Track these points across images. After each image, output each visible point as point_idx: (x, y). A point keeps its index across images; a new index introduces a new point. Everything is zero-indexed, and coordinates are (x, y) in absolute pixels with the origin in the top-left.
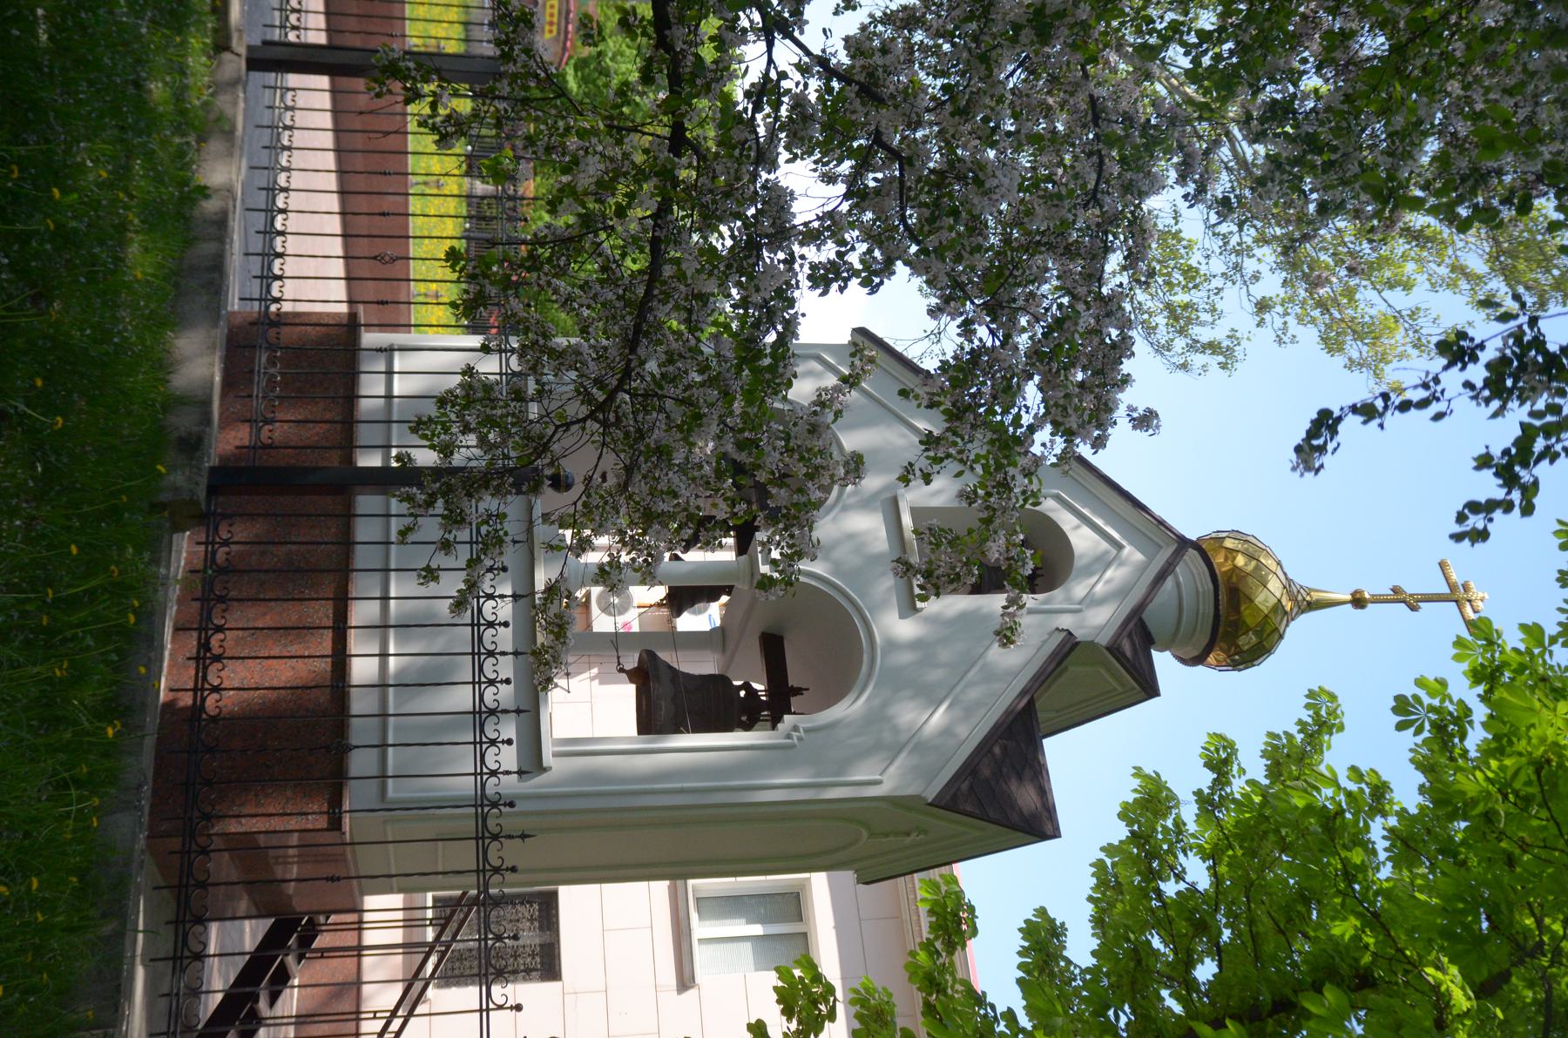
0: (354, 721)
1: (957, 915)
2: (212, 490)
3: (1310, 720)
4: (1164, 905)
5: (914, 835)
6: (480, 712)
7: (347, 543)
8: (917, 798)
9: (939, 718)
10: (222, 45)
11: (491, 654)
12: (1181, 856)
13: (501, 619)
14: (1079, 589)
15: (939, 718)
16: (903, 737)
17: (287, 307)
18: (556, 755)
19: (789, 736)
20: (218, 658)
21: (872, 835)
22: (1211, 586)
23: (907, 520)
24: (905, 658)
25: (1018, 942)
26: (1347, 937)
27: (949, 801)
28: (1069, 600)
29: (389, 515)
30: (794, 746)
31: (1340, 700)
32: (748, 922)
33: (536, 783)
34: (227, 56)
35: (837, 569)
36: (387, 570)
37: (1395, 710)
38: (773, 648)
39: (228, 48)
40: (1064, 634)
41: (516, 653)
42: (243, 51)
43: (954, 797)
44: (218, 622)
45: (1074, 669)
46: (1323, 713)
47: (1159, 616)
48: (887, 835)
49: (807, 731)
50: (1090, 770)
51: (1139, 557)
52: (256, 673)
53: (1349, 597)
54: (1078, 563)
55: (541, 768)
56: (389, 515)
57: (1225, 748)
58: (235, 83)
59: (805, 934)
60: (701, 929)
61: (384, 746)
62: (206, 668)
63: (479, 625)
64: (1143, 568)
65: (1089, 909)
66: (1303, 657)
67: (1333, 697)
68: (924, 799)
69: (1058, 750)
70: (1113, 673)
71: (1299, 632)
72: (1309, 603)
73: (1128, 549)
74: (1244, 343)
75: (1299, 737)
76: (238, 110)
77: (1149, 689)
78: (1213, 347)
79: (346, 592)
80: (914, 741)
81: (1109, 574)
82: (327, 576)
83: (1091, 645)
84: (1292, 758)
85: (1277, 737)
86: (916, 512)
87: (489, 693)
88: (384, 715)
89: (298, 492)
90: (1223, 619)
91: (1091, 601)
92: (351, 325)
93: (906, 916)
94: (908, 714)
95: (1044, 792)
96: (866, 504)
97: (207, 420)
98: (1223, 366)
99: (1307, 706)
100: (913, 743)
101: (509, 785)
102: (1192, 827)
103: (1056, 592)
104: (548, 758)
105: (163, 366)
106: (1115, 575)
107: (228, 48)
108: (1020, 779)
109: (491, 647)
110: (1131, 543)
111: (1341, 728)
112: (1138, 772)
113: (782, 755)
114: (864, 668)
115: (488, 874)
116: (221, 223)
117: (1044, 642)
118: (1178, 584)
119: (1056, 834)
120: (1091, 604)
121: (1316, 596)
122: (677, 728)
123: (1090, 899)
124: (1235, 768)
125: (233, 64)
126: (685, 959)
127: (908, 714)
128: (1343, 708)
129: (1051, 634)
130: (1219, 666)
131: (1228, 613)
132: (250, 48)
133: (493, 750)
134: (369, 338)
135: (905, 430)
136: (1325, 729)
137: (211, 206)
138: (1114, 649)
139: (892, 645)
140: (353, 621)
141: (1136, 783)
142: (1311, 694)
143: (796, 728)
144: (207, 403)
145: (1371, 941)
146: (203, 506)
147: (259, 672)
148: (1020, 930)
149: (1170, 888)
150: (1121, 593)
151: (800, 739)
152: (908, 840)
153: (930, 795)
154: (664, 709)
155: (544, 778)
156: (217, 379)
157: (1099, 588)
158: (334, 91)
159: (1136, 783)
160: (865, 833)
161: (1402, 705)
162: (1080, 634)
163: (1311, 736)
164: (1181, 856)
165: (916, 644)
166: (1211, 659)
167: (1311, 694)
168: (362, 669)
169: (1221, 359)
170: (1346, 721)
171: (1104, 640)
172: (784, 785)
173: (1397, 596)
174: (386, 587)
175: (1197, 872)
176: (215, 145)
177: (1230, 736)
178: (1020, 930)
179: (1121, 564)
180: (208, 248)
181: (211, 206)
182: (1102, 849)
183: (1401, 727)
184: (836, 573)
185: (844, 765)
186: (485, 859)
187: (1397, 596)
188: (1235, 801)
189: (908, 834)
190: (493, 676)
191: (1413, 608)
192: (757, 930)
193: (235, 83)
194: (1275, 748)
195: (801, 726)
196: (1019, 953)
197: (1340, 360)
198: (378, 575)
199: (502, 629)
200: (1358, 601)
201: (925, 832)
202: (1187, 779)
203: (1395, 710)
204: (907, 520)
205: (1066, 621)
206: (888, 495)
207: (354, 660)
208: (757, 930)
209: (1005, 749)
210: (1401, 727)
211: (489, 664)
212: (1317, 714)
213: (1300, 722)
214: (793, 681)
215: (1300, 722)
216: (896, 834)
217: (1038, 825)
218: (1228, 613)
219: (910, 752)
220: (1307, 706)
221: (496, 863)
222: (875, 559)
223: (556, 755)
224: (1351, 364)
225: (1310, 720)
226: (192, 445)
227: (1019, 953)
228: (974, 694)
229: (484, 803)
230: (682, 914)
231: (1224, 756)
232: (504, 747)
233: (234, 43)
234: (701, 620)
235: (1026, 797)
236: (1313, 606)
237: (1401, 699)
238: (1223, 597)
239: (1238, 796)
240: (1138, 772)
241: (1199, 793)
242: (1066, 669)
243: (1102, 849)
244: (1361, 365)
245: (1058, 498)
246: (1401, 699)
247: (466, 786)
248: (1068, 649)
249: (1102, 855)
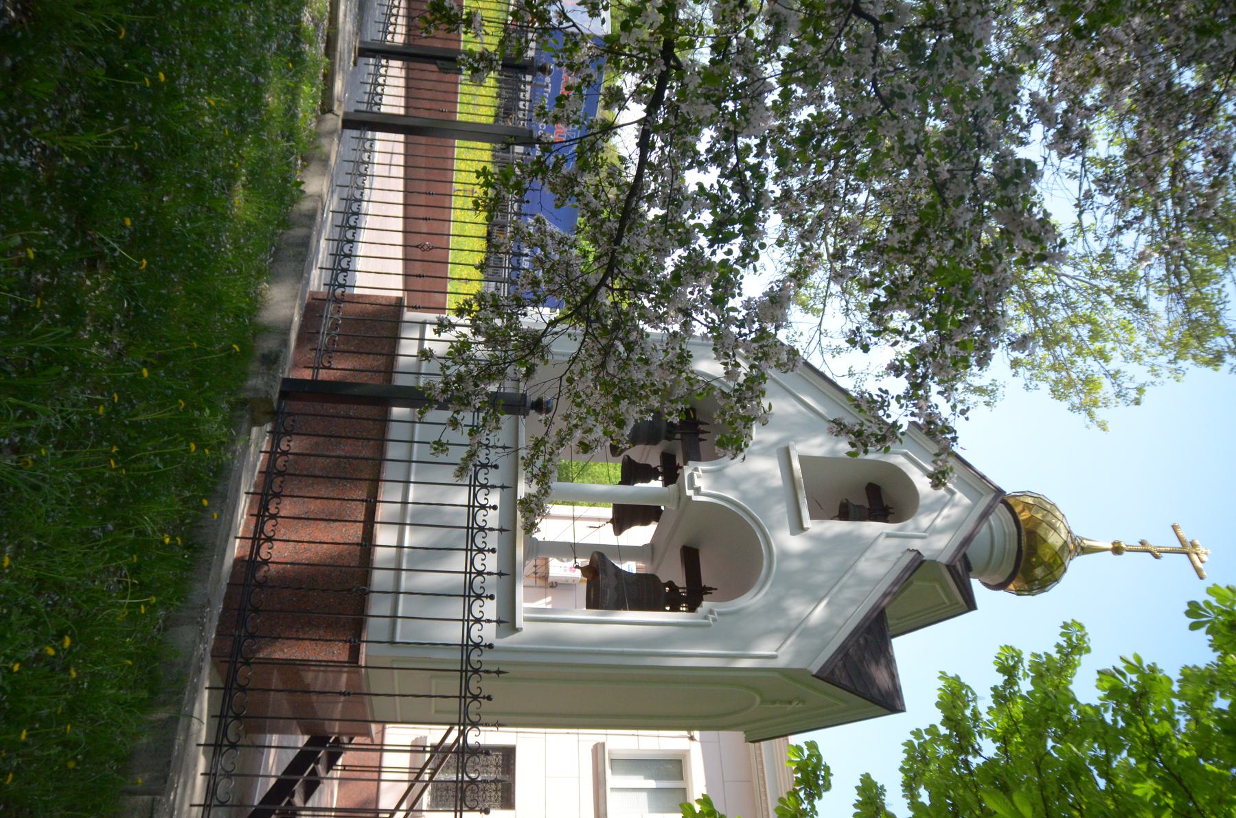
0: (371, 621)
1: (815, 773)
2: (283, 395)
3: (1065, 644)
4: (971, 773)
5: (794, 704)
6: (470, 573)
7: (379, 460)
8: (803, 671)
9: (819, 613)
10: (326, 108)
11: (482, 529)
12: (979, 739)
13: (491, 503)
14: (924, 521)
15: (819, 613)
16: (794, 624)
17: (356, 291)
18: (526, 620)
19: (706, 618)
20: (270, 539)
21: (763, 702)
22: (1015, 529)
23: (796, 464)
24: (795, 565)
25: (855, 797)
26: (1149, 797)
27: (827, 675)
28: (917, 529)
29: (412, 442)
30: (709, 625)
31: (1087, 630)
32: (646, 778)
33: (511, 640)
34: (329, 116)
35: (744, 495)
36: (408, 482)
37: (1189, 614)
38: (690, 557)
39: (331, 111)
40: (913, 554)
41: (501, 530)
42: (341, 113)
43: (832, 672)
44: (273, 510)
45: (917, 584)
46: (1074, 639)
47: (976, 552)
48: (774, 702)
49: (720, 614)
50: (924, 659)
51: (966, 501)
52: (301, 541)
53: (1111, 546)
54: (921, 503)
55: (514, 629)
56: (412, 442)
57: (1013, 657)
58: (331, 133)
59: (684, 790)
60: (613, 780)
61: (399, 570)
62: (259, 547)
63: (474, 506)
64: (970, 509)
65: (900, 777)
66: (1077, 592)
67: (1082, 627)
68: (809, 672)
69: (902, 646)
70: (936, 590)
71: (1076, 566)
72: (1083, 548)
73: (959, 495)
74: (1001, 389)
75: (1056, 656)
76: (334, 149)
77: (971, 605)
78: (980, 390)
79: (379, 473)
80: (803, 626)
81: (946, 512)
82: (363, 474)
83: (933, 563)
84: (1051, 672)
85: (1040, 656)
86: (803, 459)
87: (478, 559)
88: (394, 617)
89: (346, 404)
90: (1024, 553)
91: (933, 530)
92: (398, 305)
93: (755, 781)
94: (797, 608)
95: (893, 676)
96: (765, 452)
97: (285, 343)
98: (988, 404)
99: (1062, 635)
100: (800, 629)
101: (488, 633)
102: (985, 717)
103: (909, 522)
104: (520, 622)
105: (256, 304)
106: (950, 513)
107: (331, 111)
108: (877, 663)
109: (483, 524)
110: (960, 490)
111: (1088, 650)
112: (943, 676)
113: (700, 633)
114: (764, 571)
115: (468, 700)
116: (311, 216)
117: (899, 559)
118: (990, 527)
119: (903, 710)
120: (937, 525)
121: (1087, 543)
122: (619, 605)
123: (902, 769)
124: (1021, 672)
125: (333, 121)
126: (601, 801)
127: (797, 608)
128: (1089, 636)
129: (904, 553)
130: (1019, 592)
131: (1026, 552)
132: (346, 114)
133: (479, 602)
134: (409, 315)
135: (794, 402)
136: (1076, 651)
137: (306, 205)
138: (950, 567)
139: (785, 555)
140: (379, 517)
141: (941, 684)
142: (1065, 626)
143: (711, 612)
144: (286, 332)
145: (1171, 802)
146: (275, 405)
147: (303, 540)
148: (857, 788)
149: (975, 761)
150: (954, 526)
151: (714, 620)
152: (789, 708)
153: (815, 669)
154: (610, 595)
155: (516, 636)
156: (296, 319)
157: (939, 522)
158: (406, 143)
159: (941, 684)
160: (758, 699)
161: (1193, 610)
162: (926, 555)
163: (1066, 655)
164: (979, 739)
165: (804, 555)
166: (1011, 587)
167: (1065, 626)
168: (385, 537)
169: (987, 398)
170: (1091, 645)
171: (944, 559)
172: (700, 655)
173: (1144, 547)
174: (406, 493)
175: (989, 748)
176: (314, 167)
177: (1017, 648)
178: (857, 788)
179: (954, 505)
180: (299, 232)
181: (306, 205)
182: (912, 733)
183: (1193, 627)
184: (743, 499)
185: (749, 641)
186: (467, 688)
187: (1144, 547)
188: (1021, 697)
189: (790, 702)
190: (482, 546)
191: (1157, 557)
192: (652, 784)
193: (331, 133)
194: (1039, 664)
195: (716, 610)
196: (855, 805)
197: (1065, 404)
198: (390, 597)
199: (491, 512)
200: (1117, 550)
201: (803, 701)
202: (983, 682)
203: (1189, 614)
204: (796, 464)
205: (916, 544)
206: (783, 445)
207: (378, 549)
208: (652, 784)
209: (866, 640)
210: (1193, 627)
211: (478, 559)
212: (1070, 639)
213: (1058, 645)
214: (705, 582)
215: (1058, 645)
216: (781, 702)
217: (890, 702)
218: (1026, 552)
219: (799, 635)
220: (1062, 635)
221: (476, 692)
222: (771, 492)
223: (526, 620)
224: (1073, 408)
225: (1065, 644)
226: (271, 360)
227: (855, 805)
228: (848, 594)
229: (468, 646)
230: (600, 769)
231: (1012, 663)
232: (488, 601)
233: (335, 108)
234: (640, 535)
235: (881, 677)
236: (1086, 550)
237: (1193, 605)
238: (1024, 538)
239: (1024, 693)
240: (943, 676)
241: (994, 689)
242: (911, 583)
243: (912, 733)
244: (1079, 409)
245: (906, 455)
246: (1193, 605)
247: (454, 633)
248: (917, 565)
249: (911, 737)
